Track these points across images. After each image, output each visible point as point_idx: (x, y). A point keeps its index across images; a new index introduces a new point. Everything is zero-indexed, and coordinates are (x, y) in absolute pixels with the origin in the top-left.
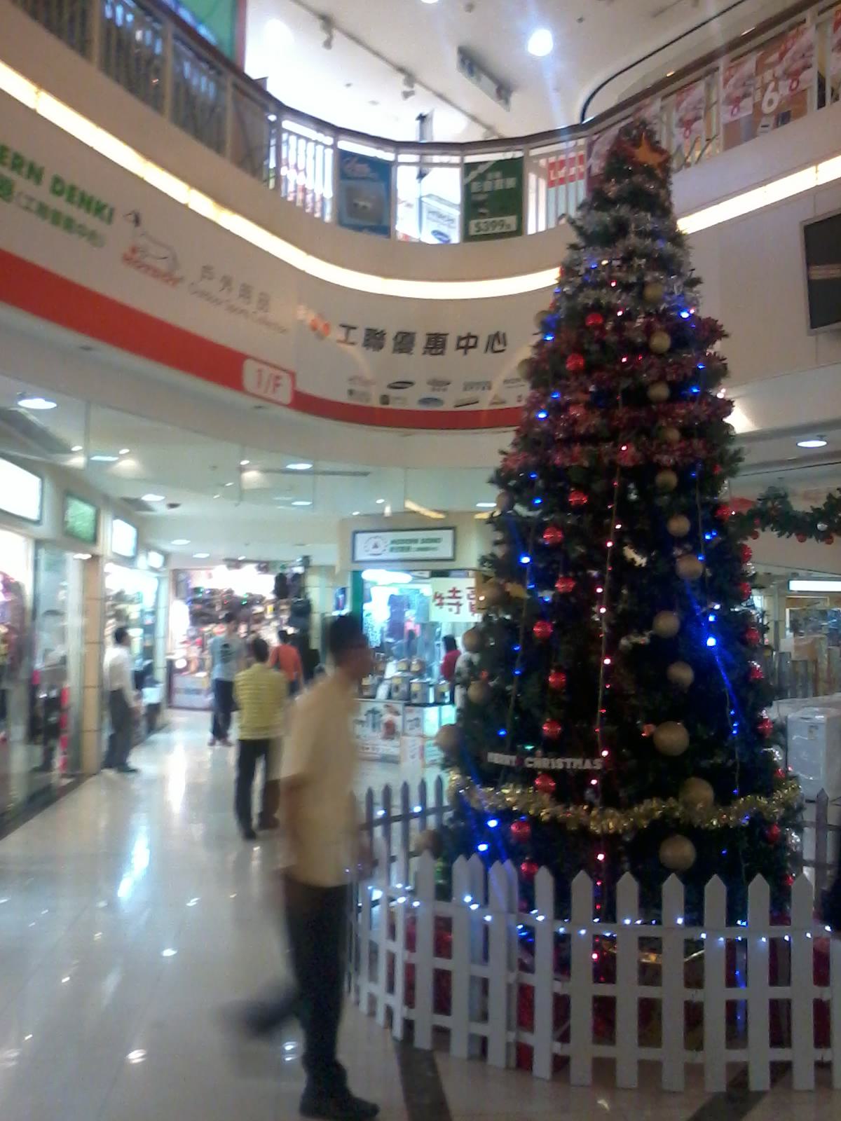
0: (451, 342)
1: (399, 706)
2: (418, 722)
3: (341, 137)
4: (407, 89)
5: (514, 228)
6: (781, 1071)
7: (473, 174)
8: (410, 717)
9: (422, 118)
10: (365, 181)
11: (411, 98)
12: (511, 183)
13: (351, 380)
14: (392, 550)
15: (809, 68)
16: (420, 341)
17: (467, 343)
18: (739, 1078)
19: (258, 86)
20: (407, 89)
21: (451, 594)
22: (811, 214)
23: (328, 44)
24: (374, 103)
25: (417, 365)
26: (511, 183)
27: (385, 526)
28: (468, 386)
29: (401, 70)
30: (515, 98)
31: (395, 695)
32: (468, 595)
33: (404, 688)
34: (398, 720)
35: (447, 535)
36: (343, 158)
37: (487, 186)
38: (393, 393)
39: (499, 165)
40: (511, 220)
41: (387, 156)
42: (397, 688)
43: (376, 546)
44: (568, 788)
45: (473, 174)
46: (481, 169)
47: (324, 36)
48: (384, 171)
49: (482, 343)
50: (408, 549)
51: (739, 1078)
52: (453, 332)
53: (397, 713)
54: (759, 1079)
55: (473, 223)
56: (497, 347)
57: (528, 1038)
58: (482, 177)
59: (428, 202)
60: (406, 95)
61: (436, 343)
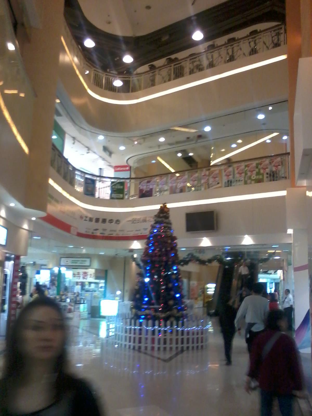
0: (107, 221)
1: (73, 304)
2: (79, 308)
3: (86, 174)
4: (88, 151)
5: (122, 197)
6: (188, 348)
7: (113, 184)
8: (76, 307)
9: (100, 169)
10: (90, 185)
11: (89, 154)
12: (122, 187)
13: (86, 228)
14: (72, 263)
15: (181, 150)
16: (101, 220)
17: (111, 221)
18: (182, 347)
19: (66, 160)
20: (88, 151)
21: (77, 274)
22: (189, 211)
23: (74, 143)
24: (77, 151)
25: (100, 226)
26: (122, 187)
27: (65, 257)
28: (111, 231)
29: (87, 147)
30: (113, 155)
31: (72, 301)
32: (82, 274)
33: (75, 299)
34: (72, 308)
35: (88, 260)
36: (86, 179)
37: (116, 187)
38: (95, 231)
39: (119, 183)
40: (121, 195)
41: (95, 178)
42: (73, 299)
43: (67, 262)
44: (156, 310)
45: (113, 184)
46: (115, 183)
47: (73, 142)
48: (93, 182)
49: (114, 221)
50: (76, 263)
51: (182, 347)
52: (108, 218)
53: (72, 306)
54: (185, 348)
55: (113, 195)
56: (118, 223)
57: (154, 345)
58: (115, 185)
59: (103, 190)
60: (88, 153)
61: (104, 221)
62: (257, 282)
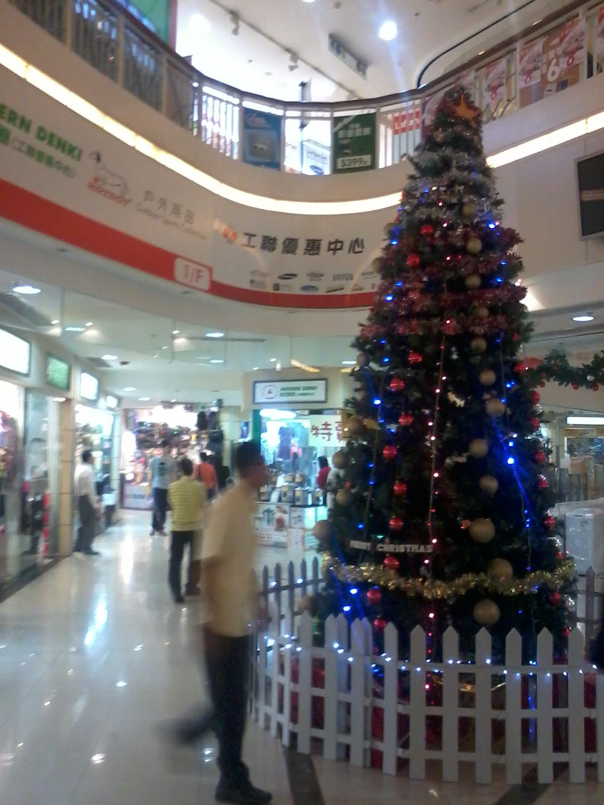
0: (324, 246)
1: (287, 507)
2: (300, 519)
3: (245, 98)
4: (292, 64)
5: (369, 164)
6: (561, 769)
7: (340, 125)
8: (294, 515)
9: (303, 85)
10: (262, 130)
11: (295, 71)
12: (367, 131)
13: (252, 273)
14: (281, 395)
15: (581, 49)
16: (302, 245)
17: (335, 246)
18: (531, 774)
19: (185, 62)
20: (292, 64)
21: (324, 427)
22: (582, 153)
23: (235, 32)
24: (269, 74)
25: (299, 262)
26: (367, 131)
27: (277, 378)
28: (336, 277)
29: (288, 50)
30: (370, 71)
31: (284, 499)
32: (336, 427)
33: (290, 494)
34: (286, 517)
35: (321, 384)
36: (247, 114)
37: (350, 133)
38: (283, 282)
39: (358, 118)
40: (367, 158)
41: (278, 112)
42: (285, 494)
43: (270, 392)
44: (408, 566)
45: (340, 125)
46: (346, 121)
47: (233, 26)
48: (276, 123)
49: (346, 246)
50: (293, 394)
51: (531, 774)
52: (326, 239)
53: (285, 512)
54: (545, 775)
55: (340, 160)
56: (357, 249)
57: (379, 746)
58: (346, 127)
59: (307, 145)
60: (292, 68)
61: (313, 247)
62: (295, 583)
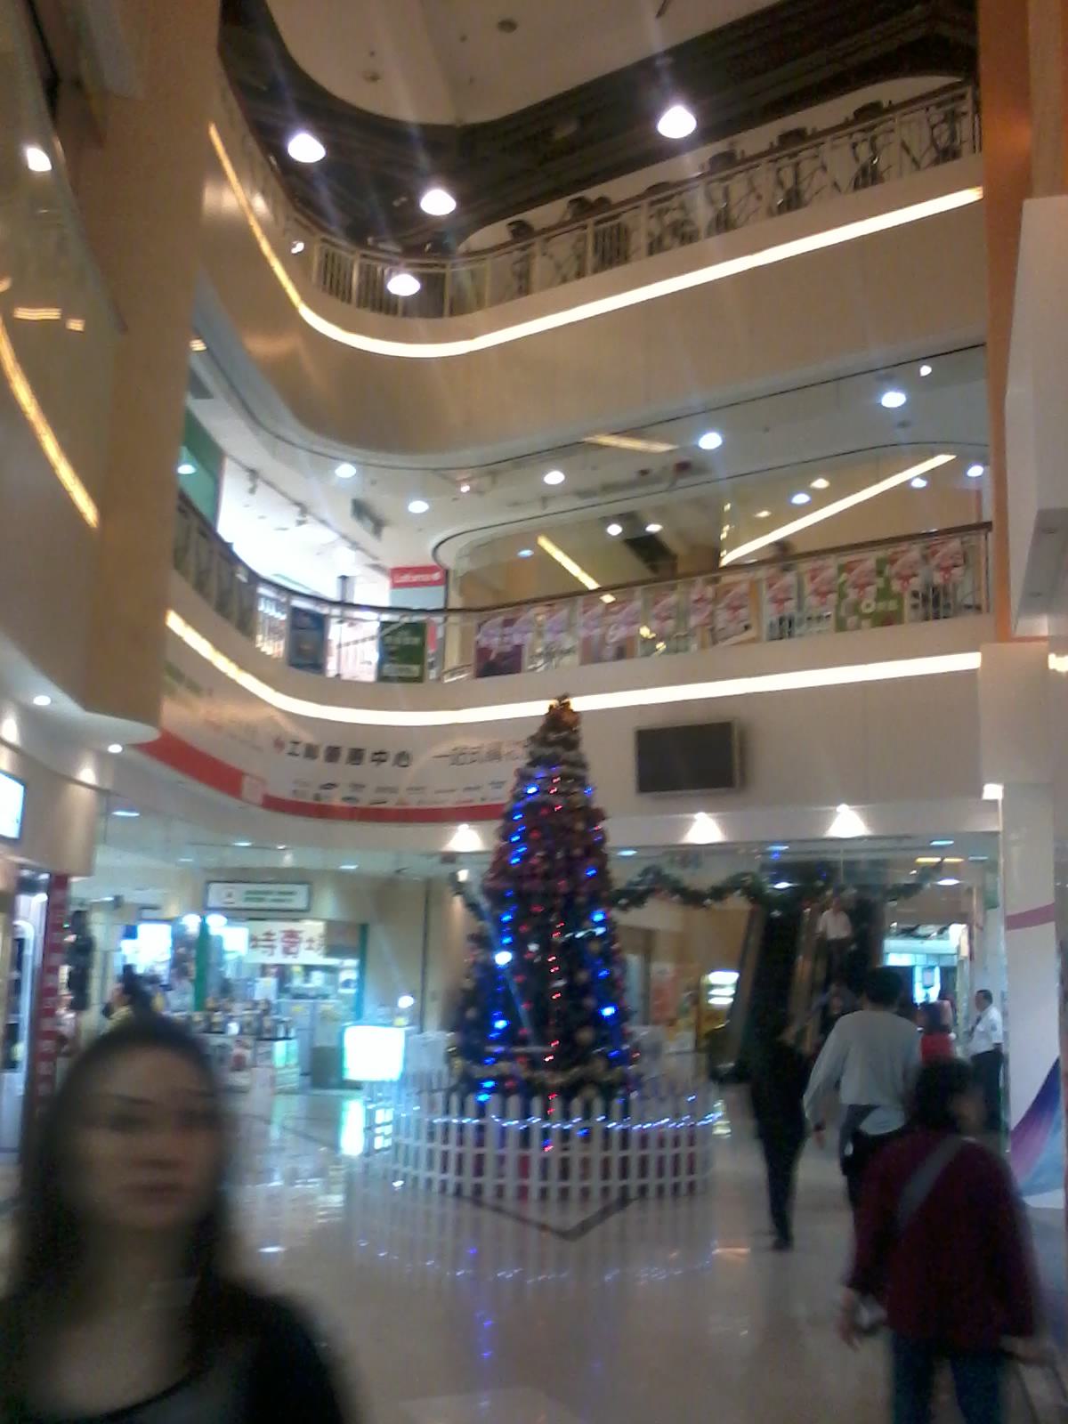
0: (368, 756)
1: (249, 1041)
2: (269, 1055)
3: (293, 597)
4: (300, 518)
5: (416, 675)
6: (643, 1190)
7: (387, 631)
8: (261, 1050)
9: (344, 578)
10: (308, 634)
11: (304, 526)
12: (416, 641)
13: (296, 782)
14: (247, 899)
15: (621, 515)
16: (345, 754)
17: (380, 757)
18: (624, 1190)
19: (227, 547)
20: (300, 518)
21: (264, 937)
22: (646, 723)
23: (252, 491)
24: (262, 517)
25: (343, 772)
26: (416, 641)
27: (222, 878)
28: (380, 789)
29: (298, 504)
30: (386, 531)
31: (246, 1030)
32: (282, 939)
33: (255, 1025)
34: (248, 1054)
35: (302, 890)
36: (296, 612)
37: (398, 640)
38: (324, 792)
39: (407, 626)
40: (415, 669)
41: (325, 610)
42: (249, 1024)
43: (230, 895)
44: (534, 1062)
45: (387, 631)
46: (394, 627)
47: (249, 485)
48: (320, 622)
49: (392, 758)
50: (261, 900)
51: (624, 1190)
52: (370, 748)
53: (247, 1047)
54: (633, 1193)
55: (387, 666)
56: (404, 763)
57: (526, 1182)
58: (393, 633)
59: (354, 651)
60: (300, 523)
61: (356, 756)
